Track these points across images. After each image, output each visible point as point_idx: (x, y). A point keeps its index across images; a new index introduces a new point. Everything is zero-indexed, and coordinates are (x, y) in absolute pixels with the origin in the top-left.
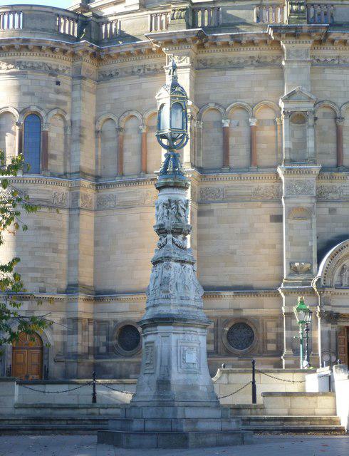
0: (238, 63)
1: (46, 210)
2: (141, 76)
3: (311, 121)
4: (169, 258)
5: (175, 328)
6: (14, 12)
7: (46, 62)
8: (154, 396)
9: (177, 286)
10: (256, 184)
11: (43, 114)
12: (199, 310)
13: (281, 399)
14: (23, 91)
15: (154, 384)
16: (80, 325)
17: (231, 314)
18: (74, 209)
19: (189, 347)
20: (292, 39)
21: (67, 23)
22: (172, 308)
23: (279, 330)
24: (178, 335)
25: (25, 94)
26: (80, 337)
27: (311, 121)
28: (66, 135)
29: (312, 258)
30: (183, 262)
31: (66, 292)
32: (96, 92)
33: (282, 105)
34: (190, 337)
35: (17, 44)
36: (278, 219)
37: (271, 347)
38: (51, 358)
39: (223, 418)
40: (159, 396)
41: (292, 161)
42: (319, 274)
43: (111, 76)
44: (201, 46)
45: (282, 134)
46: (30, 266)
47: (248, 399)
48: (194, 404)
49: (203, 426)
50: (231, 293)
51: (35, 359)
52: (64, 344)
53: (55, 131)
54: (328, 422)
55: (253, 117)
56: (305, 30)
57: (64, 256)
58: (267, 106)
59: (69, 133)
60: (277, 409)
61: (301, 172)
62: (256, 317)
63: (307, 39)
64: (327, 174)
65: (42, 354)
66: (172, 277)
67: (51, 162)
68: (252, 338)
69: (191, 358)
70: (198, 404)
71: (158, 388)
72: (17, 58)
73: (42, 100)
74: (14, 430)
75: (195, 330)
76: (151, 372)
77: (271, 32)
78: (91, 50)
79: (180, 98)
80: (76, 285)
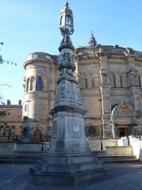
1: (43, 100)
4: (64, 78)
6: (36, 54)
8: (55, 151)
9: (68, 92)
10: (95, 92)
12: (80, 106)
13: (112, 149)
14: (37, 72)
15: (55, 143)
16: (50, 129)
17: (89, 125)
18: (49, 100)
19: (75, 123)
20: (102, 57)
22: (66, 102)
23: (102, 129)
24: (69, 117)
25: (38, 72)
26: (51, 132)
27: (108, 76)
28: (48, 82)
29: (110, 110)
30: (72, 81)
31: (47, 120)
32: (55, 73)
33: (100, 72)
34: (76, 118)
35: (36, 61)
36: (101, 100)
38: (43, 137)
39: (94, 162)
40: (58, 151)
41: (103, 85)
42: (112, 113)
44: (80, 60)
45: (100, 79)
46: (38, 113)
47: (100, 150)
48: (78, 155)
49: (83, 168)
50: (89, 119)
51: (39, 137)
52: (47, 133)
53: (45, 81)
54: (131, 158)
55: (93, 76)
56: (105, 54)
57: (47, 111)
58: (96, 73)
59: (48, 82)
60: (111, 153)
61: (106, 88)
62: (96, 126)
63: (106, 56)
64: (112, 89)
65: (41, 136)
66: (66, 87)
67: (44, 88)
69: (77, 129)
70: (81, 155)
71: (57, 146)
72: (36, 64)
73: (42, 74)
74: (10, 162)
75: (78, 115)
76: (55, 137)
77: (97, 55)
78: (54, 62)
80: (50, 119)
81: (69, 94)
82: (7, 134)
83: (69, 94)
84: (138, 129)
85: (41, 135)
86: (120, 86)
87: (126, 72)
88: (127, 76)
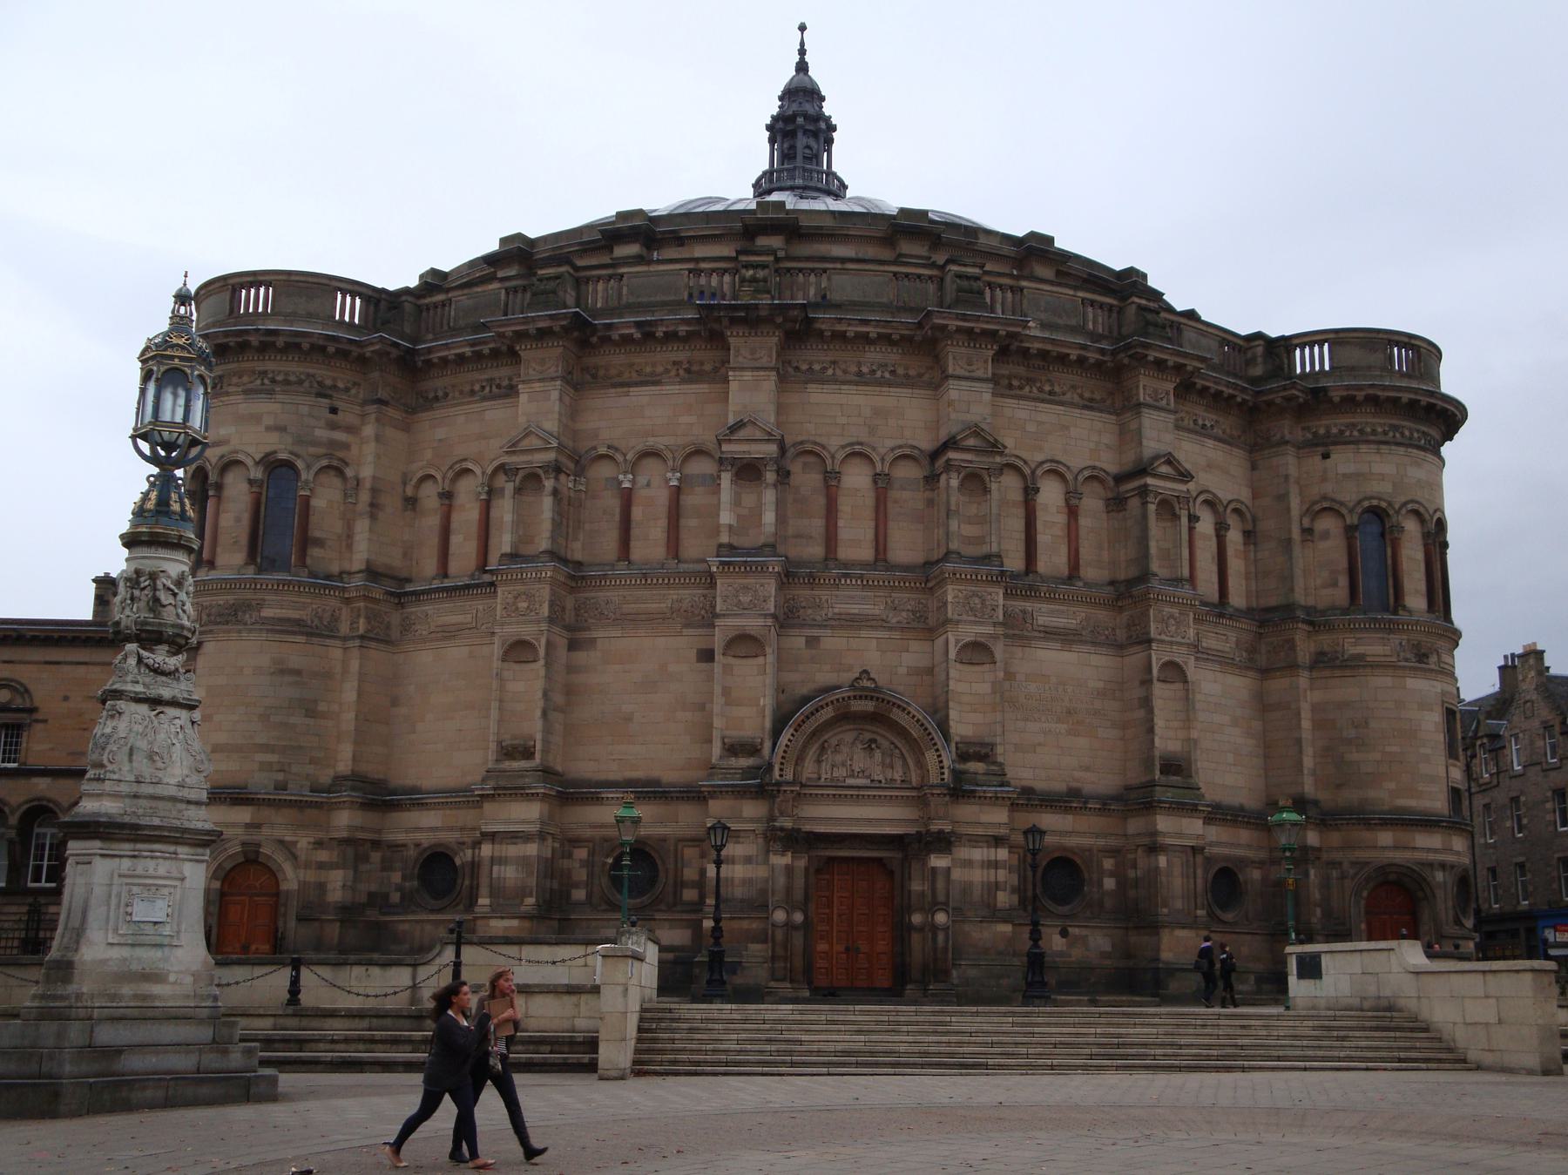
0: (653, 374)
2: (484, 399)
3: (770, 477)
5: (107, 845)
7: (311, 371)
9: (131, 755)
11: (300, 464)
21: (348, 299)
27: (770, 477)
34: (151, 864)
37: (689, 895)
43: (436, 399)
68: (653, 880)
73: (299, 441)
79: (181, 359)
81: (131, 761)
82: (38, 869)
83: (131, 761)
84: (957, 874)
85: (277, 894)
86: (866, 553)
87: (926, 443)
88: (931, 480)
